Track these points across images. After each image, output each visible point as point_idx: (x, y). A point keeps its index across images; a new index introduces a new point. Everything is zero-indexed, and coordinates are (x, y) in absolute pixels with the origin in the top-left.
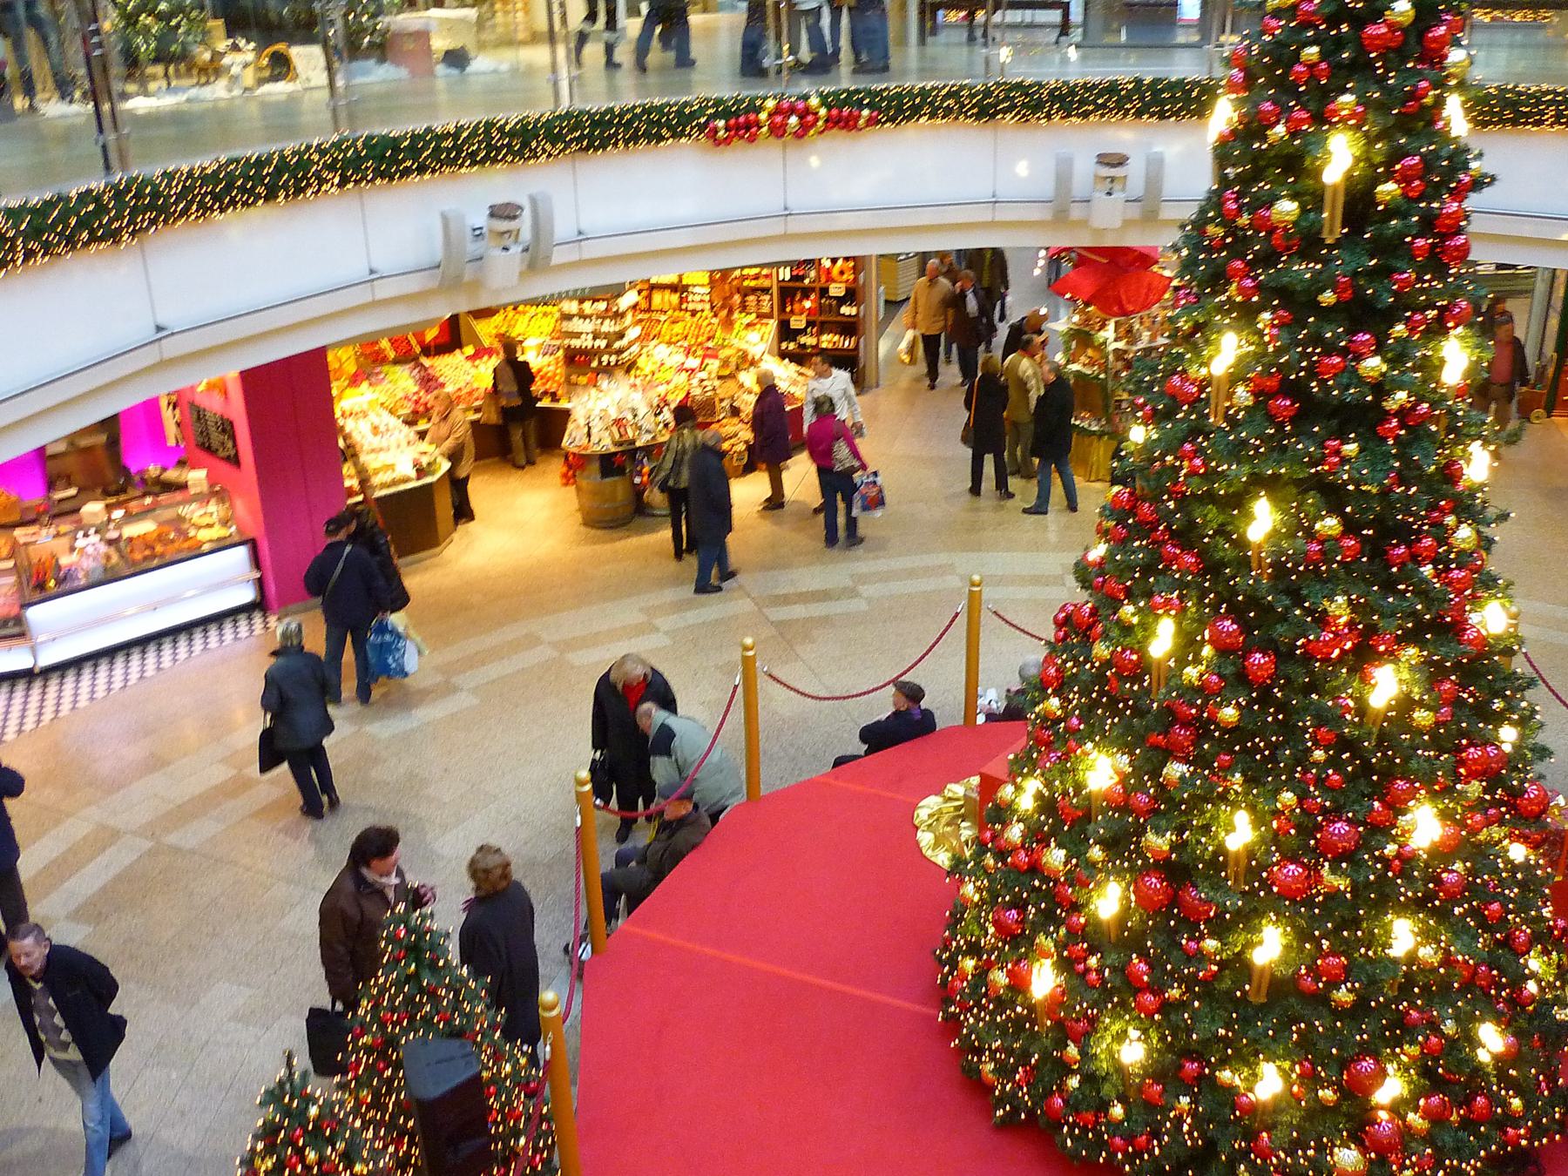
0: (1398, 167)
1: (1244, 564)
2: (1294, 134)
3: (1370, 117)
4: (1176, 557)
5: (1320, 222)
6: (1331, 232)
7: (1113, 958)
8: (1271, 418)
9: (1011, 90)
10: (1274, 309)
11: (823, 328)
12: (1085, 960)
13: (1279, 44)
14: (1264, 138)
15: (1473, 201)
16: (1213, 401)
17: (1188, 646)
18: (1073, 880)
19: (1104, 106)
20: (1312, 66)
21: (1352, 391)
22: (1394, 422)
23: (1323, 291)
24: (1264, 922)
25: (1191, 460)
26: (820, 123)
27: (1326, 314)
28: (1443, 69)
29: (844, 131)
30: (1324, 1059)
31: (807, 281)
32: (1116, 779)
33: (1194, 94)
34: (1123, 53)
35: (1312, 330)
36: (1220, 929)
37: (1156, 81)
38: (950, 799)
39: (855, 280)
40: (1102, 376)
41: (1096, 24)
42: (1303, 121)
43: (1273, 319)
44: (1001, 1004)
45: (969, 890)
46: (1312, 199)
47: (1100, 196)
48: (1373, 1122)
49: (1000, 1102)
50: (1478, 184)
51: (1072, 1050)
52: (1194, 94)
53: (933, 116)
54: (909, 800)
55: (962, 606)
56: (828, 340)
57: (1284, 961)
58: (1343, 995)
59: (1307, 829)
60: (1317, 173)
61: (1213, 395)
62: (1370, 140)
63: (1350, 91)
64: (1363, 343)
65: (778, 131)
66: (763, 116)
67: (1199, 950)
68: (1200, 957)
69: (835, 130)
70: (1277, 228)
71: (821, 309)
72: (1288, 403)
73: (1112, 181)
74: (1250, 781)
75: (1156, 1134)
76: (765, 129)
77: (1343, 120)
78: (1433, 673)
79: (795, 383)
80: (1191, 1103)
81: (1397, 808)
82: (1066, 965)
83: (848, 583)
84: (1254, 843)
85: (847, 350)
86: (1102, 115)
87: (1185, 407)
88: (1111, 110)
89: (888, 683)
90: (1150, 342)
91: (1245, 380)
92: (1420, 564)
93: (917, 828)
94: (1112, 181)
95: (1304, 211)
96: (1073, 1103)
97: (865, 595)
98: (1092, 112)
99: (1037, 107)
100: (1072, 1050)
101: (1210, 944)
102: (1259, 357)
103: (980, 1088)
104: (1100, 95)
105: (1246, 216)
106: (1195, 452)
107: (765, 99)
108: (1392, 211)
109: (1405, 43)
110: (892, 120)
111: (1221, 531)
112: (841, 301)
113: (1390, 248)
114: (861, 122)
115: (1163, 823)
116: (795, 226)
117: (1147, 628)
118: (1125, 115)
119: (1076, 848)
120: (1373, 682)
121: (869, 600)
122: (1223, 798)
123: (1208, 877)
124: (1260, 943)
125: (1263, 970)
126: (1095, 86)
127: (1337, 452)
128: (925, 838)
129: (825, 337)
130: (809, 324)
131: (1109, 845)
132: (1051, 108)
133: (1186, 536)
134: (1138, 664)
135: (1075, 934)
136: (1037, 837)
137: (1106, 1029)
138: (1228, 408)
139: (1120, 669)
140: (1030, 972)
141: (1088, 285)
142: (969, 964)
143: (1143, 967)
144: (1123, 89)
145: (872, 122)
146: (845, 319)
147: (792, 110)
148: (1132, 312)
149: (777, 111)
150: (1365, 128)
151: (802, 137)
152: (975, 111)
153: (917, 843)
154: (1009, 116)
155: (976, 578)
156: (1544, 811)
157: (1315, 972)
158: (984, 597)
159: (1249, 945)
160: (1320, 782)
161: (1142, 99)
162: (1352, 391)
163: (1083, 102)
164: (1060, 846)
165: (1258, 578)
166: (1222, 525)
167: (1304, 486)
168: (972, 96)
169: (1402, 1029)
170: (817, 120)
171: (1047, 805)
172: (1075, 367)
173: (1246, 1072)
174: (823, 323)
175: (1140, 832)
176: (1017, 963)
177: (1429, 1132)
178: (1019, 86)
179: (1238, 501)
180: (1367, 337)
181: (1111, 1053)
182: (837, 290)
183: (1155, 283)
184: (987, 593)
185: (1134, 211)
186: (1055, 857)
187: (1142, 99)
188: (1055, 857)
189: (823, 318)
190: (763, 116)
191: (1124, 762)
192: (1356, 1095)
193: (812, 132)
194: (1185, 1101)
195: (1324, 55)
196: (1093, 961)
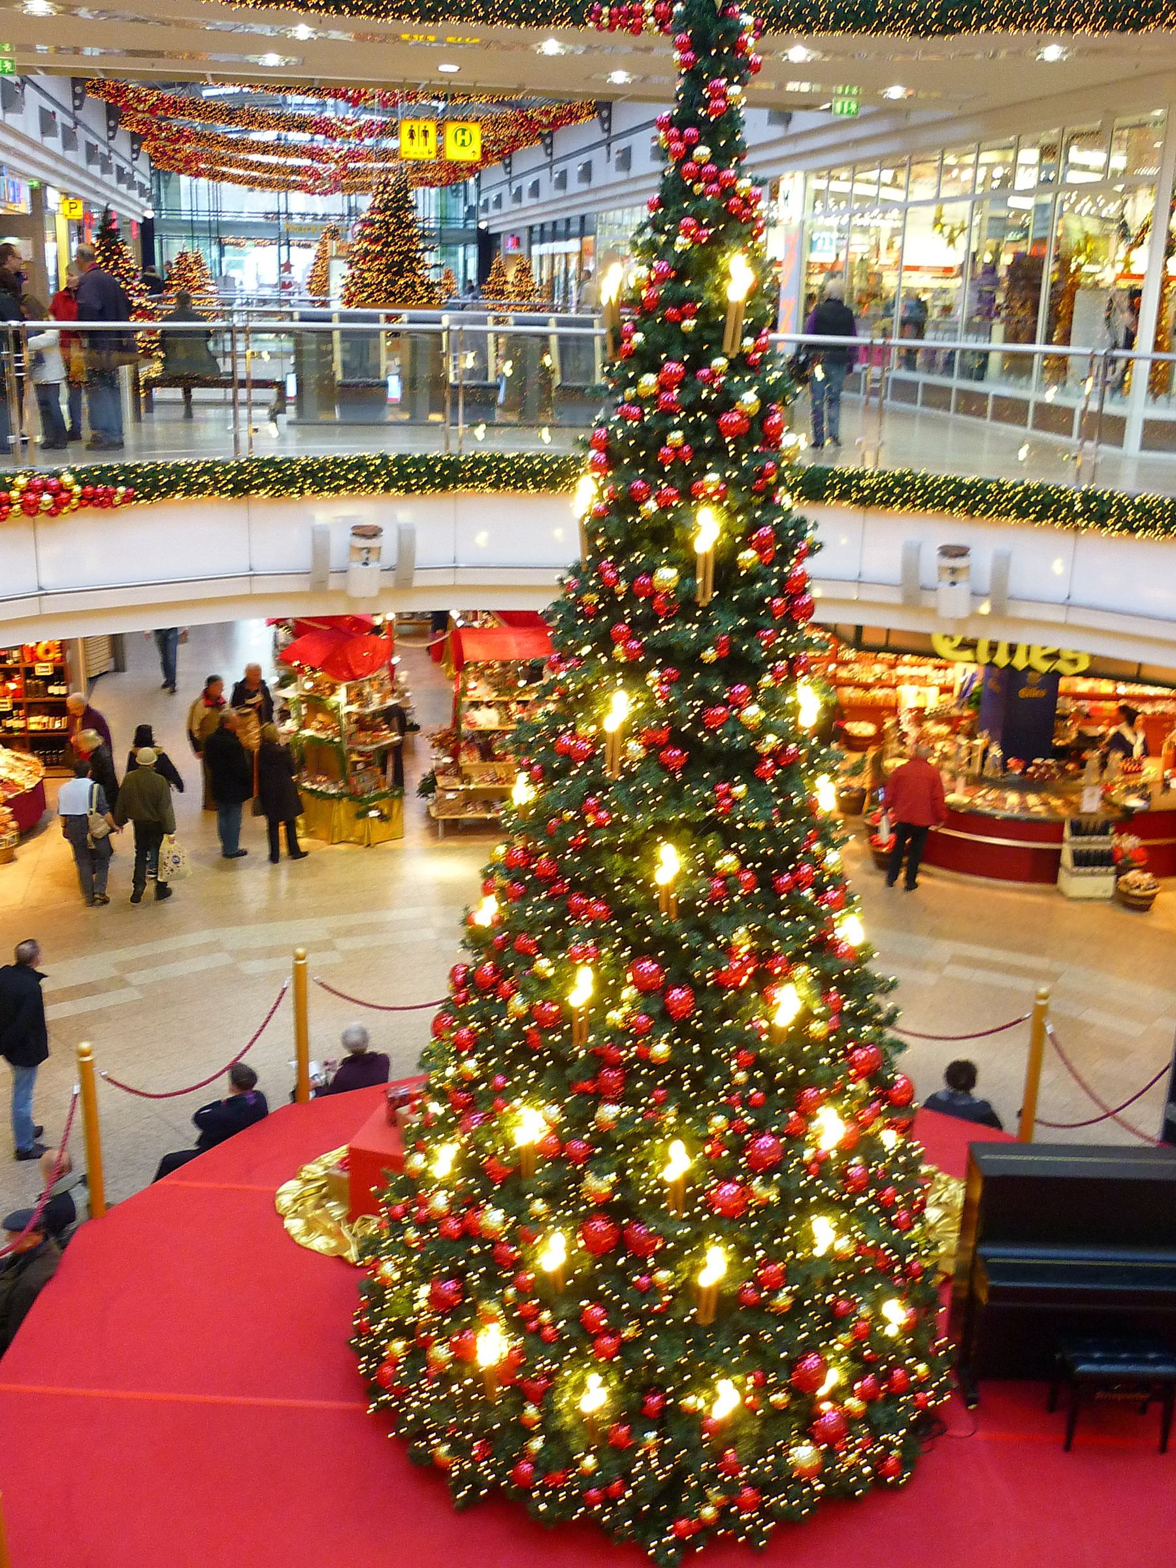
0: (754, 537)
1: (653, 907)
2: (665, 508)
3: (730, 494)
4: (586, 908)
5: (694, 587)
6: (704, 594)
7: (564, 1310)
8: (664, 767)
9: (263, 466)
10: (660, 668)
11: (32, 709)
12: (536, 1316)
13: (645, 429)
14: (638, 513)
15: (809, 566)
16: (608, 757)
17: (608, 994)
18: (515, 1237)
19: (354, 481)
20: (677, 450)
21: (739, 738)
22: (769, 763)
23: (705, 648)
24: (706, 1244)
25: (595, 814)
26: (74, 501)
27: (707, 669)
28: (779, 451)
29: (98, 509)
30: (774, 1365)
31: (9, 662)
32: (548, 1129)
33: (437, 469)
34: (338, 429)
35: (698, 685)
36: (666, 1260)
37: (400, 457)
38: (309, 1181)
39: (63, 658)
40: (337, 740)
41: (311, 402)
42: (672, 497)
43: (661, 677)
44: (446, 1380)
45: (388, 1269)
46: (688, 568)
47: (357, 566)
48: (820, 1415)
49: (460, 1482)
50: (811, 550)
51: (531, 1411)
52: (437, 469)
53: (187, 492)
54: (266, 1188)
55: (288, 982)
56: (36, 723)
57: (730, 1278)
58: (783, 1300)
59: (739, 1148)
60: (687, 545)
61: (608, 751)
62: (732, 513)
63: (711, 470)
64: (740, 694)
65: (31, 509)
66: (15, 494)
67: (652, 1284)
68: (653, 1290)
69: (89, 508)
70: (659, 593)
71: (27, 690)
72: (677, 753)
73: (369, 552)
74: (683, 1112)
75: (627, 1478)
76: (17, 507)
77: (708, 497)
78: (823, 983)
79: (13, 770)
80: (657, 1437)
81: (807, 1115)
82: (518, 1325)
83: (114, 972)
84: (693, 1171)
85: (57, 730)
86: (353, 490)
87: (580, 764)
88: (361, 484)
89: (223, 1071)
90: (381, 703)
91: (637, 735)
92: (802, 889)
93: (282, 1217)
94: (369, 552)
95: (682, 578)
96: (540, 1464)
97: (135, 982)
98: (342, 486)
99: (289, 482)
100: (531, 1411)
101: (663, 1276)
102: (651, 710)
103: (434, 1472)
104: (349, 470)
105: (623, 583)
106: (598, 805)
107: (14, 476)
108: (752, 578)
109: (751, 428)
110: (148, 497)
111: (626, 879)
112: (49, 681)
113: (750, 607)
114: (117, 499)
115: (605, 1166)
116: (51, 606)
117: (565, 979)
118: (374, 489)
119: (514, 1202)
120: (774, 1002)
121: (141, 987)
122: (657, 1133)
123: (650, 1212)
124: (705, 1265)
125: (710, 1290)
126: (344, 462)
127: (728, 795)
128: (294, 1226)
129: (32, 719)
130: (16, 706)
131: (550, 1196)
132: (304, 482)
133: (597, 886)
134: (558, 1015)
135: (524, 1292)
136: (468, 1202)
137: (565, 1382)
138: (624, 761)
139: (541, 1021)
140: (474, 1342)
141: (318, 652)
142: (398, 1346)
143: (598, 1312)
144: (371, 465)
145: (127, 499)
146: (53, 699)
147: (45, 488)
148: (361, 676)
149: (30, 488)
150: (726, 503)
151: (56, 514)
152: (230, 486)
153: (286, 1231)
154: (262, 492)
155: (300, 951)
156: (911, 1100)
157: (759, 1284)
158: (309, 965)
159: (694, 1269)
160: (746, 1102)
161: (389, 474)
162: (739, 738)
163: (334, 477)
164: (497, 1206)
165: (664, 920)
166: (626, 872)
167: (701, 829)
168: (226, 472)
169: (835, 1320)
170: (71, 497)
171: (470, 1166)
172: (307, 733)
173: (706, 1394)
174: (30, 704)
175: (579, 1178)
176: (461, 1334)
177: (866, 1411)
178: (271, 462)
179: (640, 847)
180: (743, 688)
181: (572, 1405)
182: (43, 669)
183: (379, 647)
184: (313, 961)
185: (389, 580)
186: (493, 1218)
187: (389, 474)
188: (493, 1218)
189: (29, 700)
190: (15, 494)
191: (554, 1112)
192: (803, 1390)
193: (65, 509)
194: (651, 1436)
195: (686, 439)
196: (546, 1316)
